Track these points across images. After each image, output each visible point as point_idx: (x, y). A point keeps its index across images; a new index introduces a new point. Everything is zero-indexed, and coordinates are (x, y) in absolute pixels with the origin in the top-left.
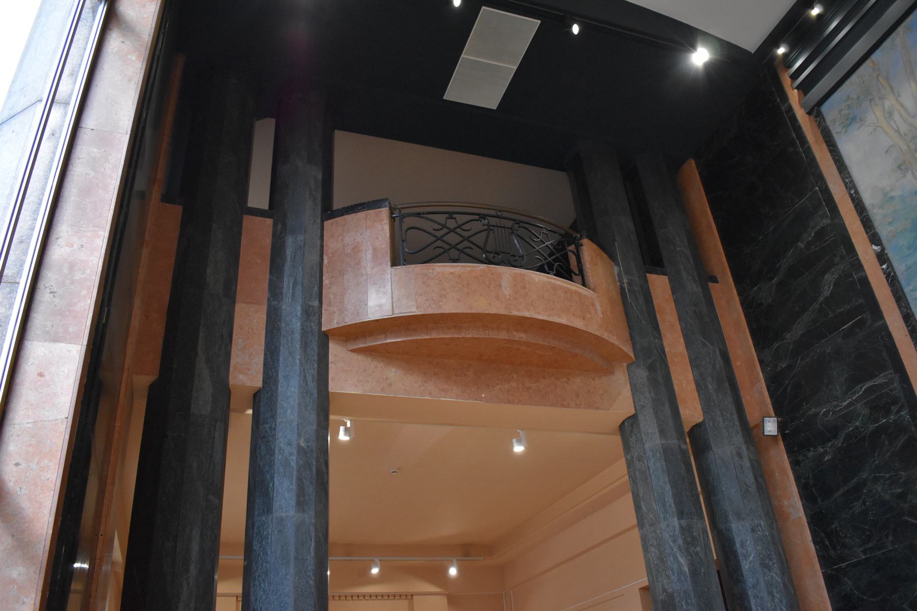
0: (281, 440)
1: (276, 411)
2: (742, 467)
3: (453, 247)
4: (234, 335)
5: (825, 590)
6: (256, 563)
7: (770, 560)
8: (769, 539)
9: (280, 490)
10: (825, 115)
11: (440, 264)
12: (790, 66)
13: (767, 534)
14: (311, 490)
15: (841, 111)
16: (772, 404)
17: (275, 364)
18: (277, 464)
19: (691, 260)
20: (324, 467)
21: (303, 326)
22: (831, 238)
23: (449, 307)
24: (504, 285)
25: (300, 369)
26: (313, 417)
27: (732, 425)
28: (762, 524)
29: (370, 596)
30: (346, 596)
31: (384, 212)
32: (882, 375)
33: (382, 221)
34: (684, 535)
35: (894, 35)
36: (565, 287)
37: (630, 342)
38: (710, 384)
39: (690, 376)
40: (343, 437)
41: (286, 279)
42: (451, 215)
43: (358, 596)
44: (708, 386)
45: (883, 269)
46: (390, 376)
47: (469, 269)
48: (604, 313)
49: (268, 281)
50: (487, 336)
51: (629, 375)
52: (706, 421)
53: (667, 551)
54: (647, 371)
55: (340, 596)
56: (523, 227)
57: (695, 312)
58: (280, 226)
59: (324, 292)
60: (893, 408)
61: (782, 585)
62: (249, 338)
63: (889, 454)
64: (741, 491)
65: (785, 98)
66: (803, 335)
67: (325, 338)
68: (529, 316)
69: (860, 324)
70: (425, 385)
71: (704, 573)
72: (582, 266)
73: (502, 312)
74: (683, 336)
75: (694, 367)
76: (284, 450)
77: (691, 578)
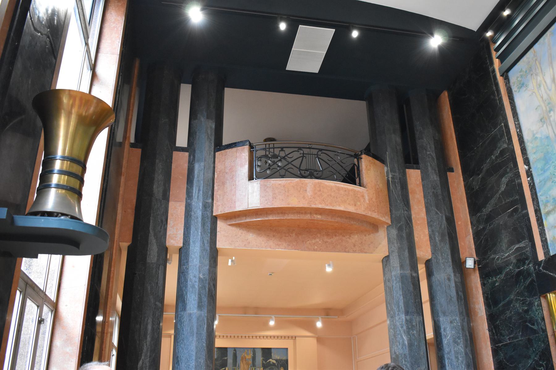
0: (191, 274)
1: (189, 260)
2: (449, 286)
5: (492, 357)
7: (459, 339)
8: (460, 327)
9: (190, 300)
10: (510, 79)
12: (495, 43)
14: (205, 300)
15: (517, 78)
16: (475, 249)
18: (189, 286)
19: (435, 160)
20: (212, 287)
21: (203, 214)
22: (507, 156)
24: (308, 189)
26: (207, 262)
28: (457, 319)
29: (271, 337)
30: (256, 337)
31: (246, 148)
32: (523, 242)
35: (545, 35)
36: (345, 188)
37: (389, 213)
38: (437, 237)
39: (426, 231)
41: (194, 188)
43: (263, 337)
44: (436, 238)
45: (528, 180)
47: (289, 181)
48: (370, 199)
50: (299, 218)
51: (387, 233)
52: (433, 258)
54: (397, 231)
56: (324, 153)
57: (433, 192)
58: (192, 157)
59: (215, 193)
60: (526, 261)
61: (464, 353)
63: (523, 287)
65: (492, 63)
66: (491, 211)
67: (215, 219)
68: (321, 207)
69: (516, 210)
70: (268, 242)
71: (417, 345)
72: (359, 172)
73: (306, 205)
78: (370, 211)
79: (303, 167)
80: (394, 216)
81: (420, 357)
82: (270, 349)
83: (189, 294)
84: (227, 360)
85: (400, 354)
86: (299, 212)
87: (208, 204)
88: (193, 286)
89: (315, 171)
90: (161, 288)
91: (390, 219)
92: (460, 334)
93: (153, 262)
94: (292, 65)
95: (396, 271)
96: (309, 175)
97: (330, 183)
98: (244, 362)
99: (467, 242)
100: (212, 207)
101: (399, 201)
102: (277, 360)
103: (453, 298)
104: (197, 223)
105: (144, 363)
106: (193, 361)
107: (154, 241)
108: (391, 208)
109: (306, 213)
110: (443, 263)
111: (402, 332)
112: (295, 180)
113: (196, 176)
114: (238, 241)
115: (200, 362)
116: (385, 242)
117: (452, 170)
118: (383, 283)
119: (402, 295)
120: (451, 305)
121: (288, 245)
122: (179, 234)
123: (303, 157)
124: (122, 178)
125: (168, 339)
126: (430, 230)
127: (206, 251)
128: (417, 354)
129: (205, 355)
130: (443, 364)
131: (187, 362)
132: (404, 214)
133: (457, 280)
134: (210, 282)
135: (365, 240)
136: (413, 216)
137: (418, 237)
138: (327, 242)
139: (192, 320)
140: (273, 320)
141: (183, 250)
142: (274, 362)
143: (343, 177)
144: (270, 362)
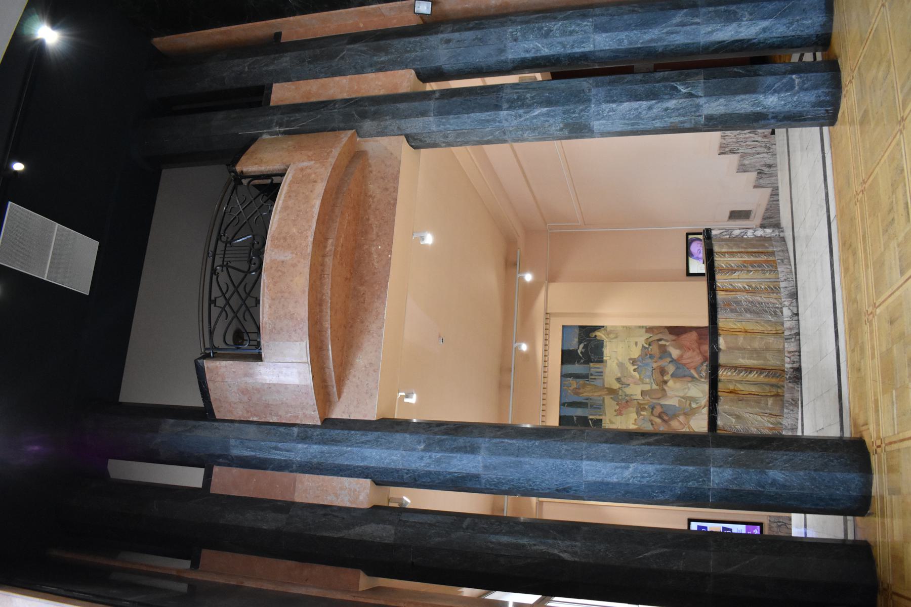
0: (417, 465)
1: (393, 469)
2: (459, 41)
3: (244, 302)
4: (323, 503)
6: (520, 488)
7: (542, 28)
9: (461, 467)
11: (261, 317)
13: (519, 27)
14: (461, 441)
17: (350, 468)
18: (438, 469)
19: (258, 58)
20: (443, 428)
21: (316, 443)
23: (302, 311)
24: (282, 258)
25: (356, 447)
26: (399, 437)
27: (419, 44)
28: (510, 30)
31: (208, 364)
33: (217, 367)
34: (516, 107)
36: (285, 197)
37: (337, 132)
38: (381, 58)
40: (413, 400)
41: (273, 457)
42: (212, 302)
44: (382, 61)
46: (363, 363)
47: (266, 290)
48: (310, 159)
49: (273, 472)
50: (330, 277)
52: (414, 67)
53: (529, 124)
55: (544, 377)
57: (309, 62)
61: (565, 22)
62: (326, 490)
64: (480, 45)
67: (328, 423)
68: (313, 237)
70: (371, 332)
72: (264, 175)
73: (308, 262)
74: (333, 77)
75: (363, 71)
76: (427, 463)
77: (553, 107)
78: (327, 159)
79: (245, 267)
80: (342, 125)
81: (569, 88)
82: (563, 351)
83: (451, 469)
84: (578, 417)
85: (564, 121)
86: (321, 275)
87: (301, 433)
88: (438, 461)
89: (253, 247)
90: (439, 518)
91: (347, 131)
92: (534, 27)
93: (393, 532)
94: (82, 283)
95: (428, 124)
96: (259, 256)
97: (274, 221)
98: (581, 391)
99: (393, 13)
100: (306, 427)
101: (319, 116)
102: (580, 343)
103: (477, 36)
104: (331, 453)
105: (565, 549)
106: (564, 463)
107: (358, 530)
108: (329, 129)
109: (323, 265)
110: (422, 50)
111: (528, 117)
112: (264, 280)
113: (253, 454)
114: (367, 383)
115: (567, 450)
116: (384, 141)
117: (278, 35)
118: (452, 148)
119: (469, 115)
120: (489, 39)
121: (379, 297)
122: (349, 485)
123: (227, 267)
124: (247, 585)
125: (545, 506)
126: (369, 70)
127: (379, 437)
128: (563, 92)
129: (555, 442)
130: (581, 56)
131: (566, 473)
132: (340, 108)
133: (449, 30)
134: (432, 431)
135: (379, 172)
136: (345, 96)
137: (380, 90)
138: (377, 233)
139: (494, 464)
140: (520, 345)
141: (378, 479)
142: (582, 346)
143: (268, 200)
144: (581, 353)
